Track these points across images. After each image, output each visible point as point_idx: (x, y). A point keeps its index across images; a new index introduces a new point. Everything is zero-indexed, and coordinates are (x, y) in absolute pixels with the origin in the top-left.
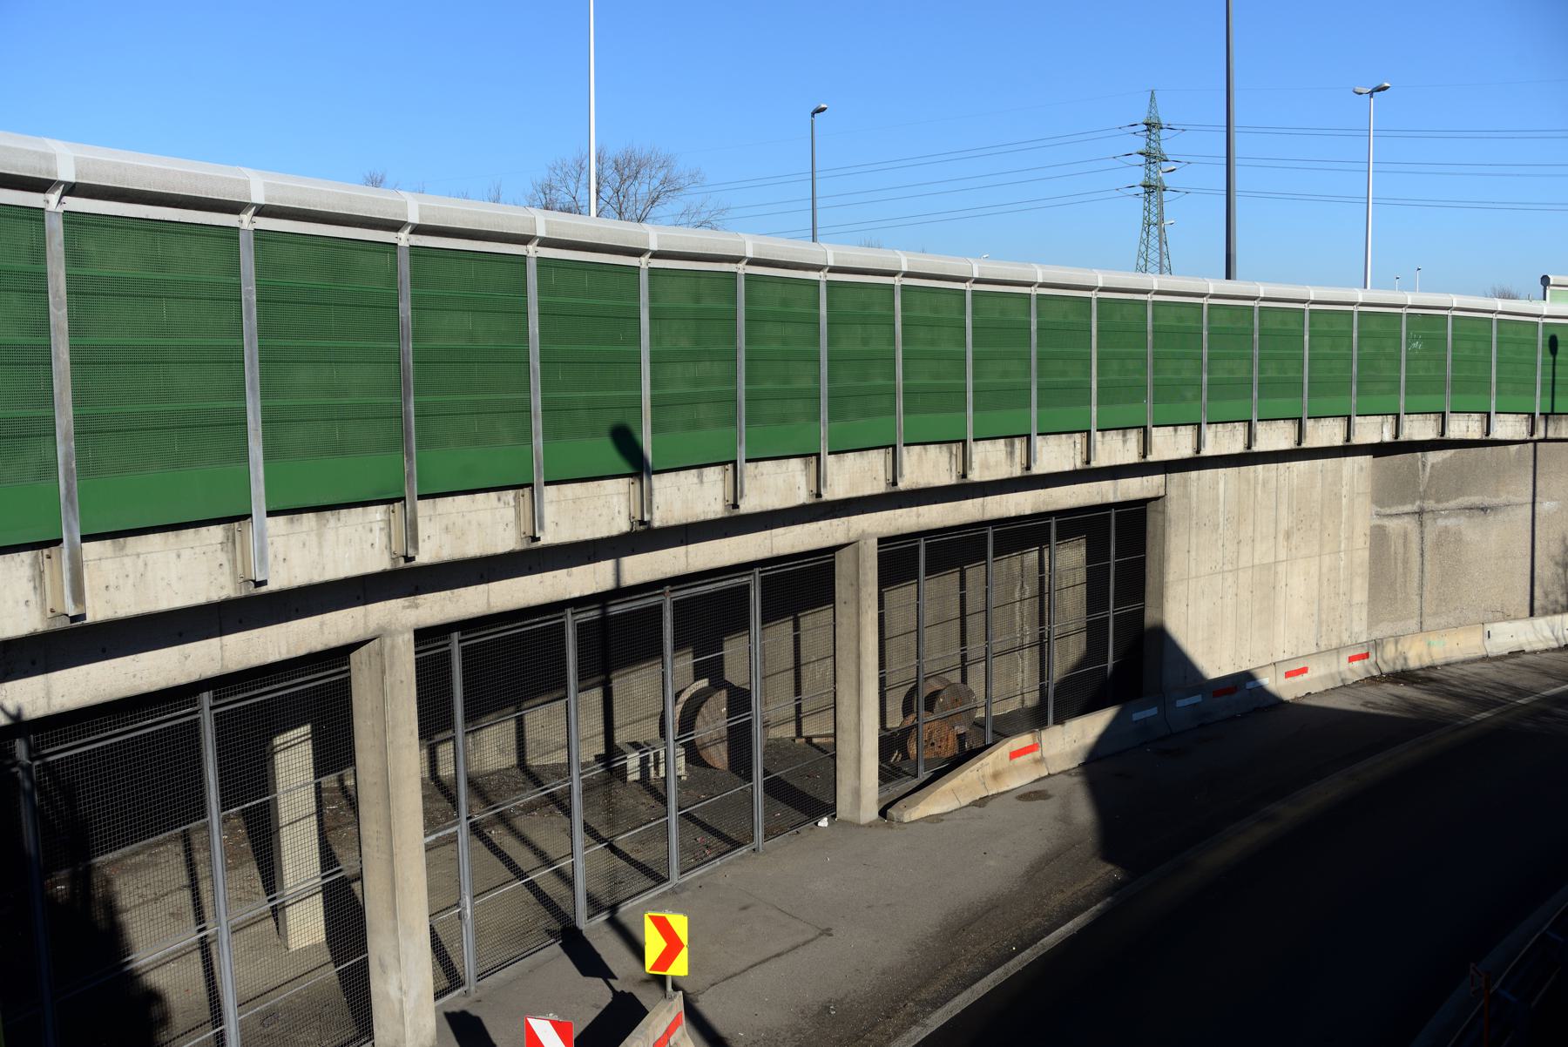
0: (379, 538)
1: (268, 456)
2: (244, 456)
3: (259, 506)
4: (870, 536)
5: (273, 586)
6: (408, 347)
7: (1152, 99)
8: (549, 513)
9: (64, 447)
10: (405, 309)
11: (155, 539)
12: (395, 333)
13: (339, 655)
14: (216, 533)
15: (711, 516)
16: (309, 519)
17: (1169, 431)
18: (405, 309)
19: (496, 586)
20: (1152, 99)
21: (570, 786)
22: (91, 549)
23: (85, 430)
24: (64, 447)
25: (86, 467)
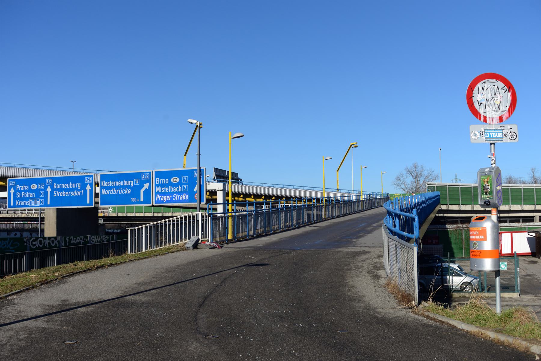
0: (471, 208)
1: (461, 201)
2: (459, 201)
3: (460, 204)
4: (538, 216)
5: (462, 209)
6: (473, 194)
7: (456, 174)
8: (537, 207)
9: (448, 199)
10: (472, 192)
11: (454, 205)
12: (471, 193)
13: (534, 217)
14: (458, 205)
15: (507, 210)
16: (465, 205)
17: (525, 208)
18: (472, 192)
19: (472, 214)
20: (456, 174)
21: (238, 233)
22: (449, 205)
23: (449, 199)
24: (448, 199)
25: (449, 201)
